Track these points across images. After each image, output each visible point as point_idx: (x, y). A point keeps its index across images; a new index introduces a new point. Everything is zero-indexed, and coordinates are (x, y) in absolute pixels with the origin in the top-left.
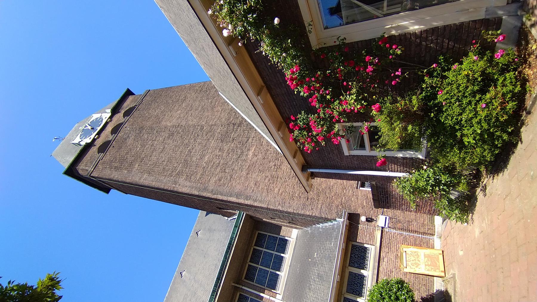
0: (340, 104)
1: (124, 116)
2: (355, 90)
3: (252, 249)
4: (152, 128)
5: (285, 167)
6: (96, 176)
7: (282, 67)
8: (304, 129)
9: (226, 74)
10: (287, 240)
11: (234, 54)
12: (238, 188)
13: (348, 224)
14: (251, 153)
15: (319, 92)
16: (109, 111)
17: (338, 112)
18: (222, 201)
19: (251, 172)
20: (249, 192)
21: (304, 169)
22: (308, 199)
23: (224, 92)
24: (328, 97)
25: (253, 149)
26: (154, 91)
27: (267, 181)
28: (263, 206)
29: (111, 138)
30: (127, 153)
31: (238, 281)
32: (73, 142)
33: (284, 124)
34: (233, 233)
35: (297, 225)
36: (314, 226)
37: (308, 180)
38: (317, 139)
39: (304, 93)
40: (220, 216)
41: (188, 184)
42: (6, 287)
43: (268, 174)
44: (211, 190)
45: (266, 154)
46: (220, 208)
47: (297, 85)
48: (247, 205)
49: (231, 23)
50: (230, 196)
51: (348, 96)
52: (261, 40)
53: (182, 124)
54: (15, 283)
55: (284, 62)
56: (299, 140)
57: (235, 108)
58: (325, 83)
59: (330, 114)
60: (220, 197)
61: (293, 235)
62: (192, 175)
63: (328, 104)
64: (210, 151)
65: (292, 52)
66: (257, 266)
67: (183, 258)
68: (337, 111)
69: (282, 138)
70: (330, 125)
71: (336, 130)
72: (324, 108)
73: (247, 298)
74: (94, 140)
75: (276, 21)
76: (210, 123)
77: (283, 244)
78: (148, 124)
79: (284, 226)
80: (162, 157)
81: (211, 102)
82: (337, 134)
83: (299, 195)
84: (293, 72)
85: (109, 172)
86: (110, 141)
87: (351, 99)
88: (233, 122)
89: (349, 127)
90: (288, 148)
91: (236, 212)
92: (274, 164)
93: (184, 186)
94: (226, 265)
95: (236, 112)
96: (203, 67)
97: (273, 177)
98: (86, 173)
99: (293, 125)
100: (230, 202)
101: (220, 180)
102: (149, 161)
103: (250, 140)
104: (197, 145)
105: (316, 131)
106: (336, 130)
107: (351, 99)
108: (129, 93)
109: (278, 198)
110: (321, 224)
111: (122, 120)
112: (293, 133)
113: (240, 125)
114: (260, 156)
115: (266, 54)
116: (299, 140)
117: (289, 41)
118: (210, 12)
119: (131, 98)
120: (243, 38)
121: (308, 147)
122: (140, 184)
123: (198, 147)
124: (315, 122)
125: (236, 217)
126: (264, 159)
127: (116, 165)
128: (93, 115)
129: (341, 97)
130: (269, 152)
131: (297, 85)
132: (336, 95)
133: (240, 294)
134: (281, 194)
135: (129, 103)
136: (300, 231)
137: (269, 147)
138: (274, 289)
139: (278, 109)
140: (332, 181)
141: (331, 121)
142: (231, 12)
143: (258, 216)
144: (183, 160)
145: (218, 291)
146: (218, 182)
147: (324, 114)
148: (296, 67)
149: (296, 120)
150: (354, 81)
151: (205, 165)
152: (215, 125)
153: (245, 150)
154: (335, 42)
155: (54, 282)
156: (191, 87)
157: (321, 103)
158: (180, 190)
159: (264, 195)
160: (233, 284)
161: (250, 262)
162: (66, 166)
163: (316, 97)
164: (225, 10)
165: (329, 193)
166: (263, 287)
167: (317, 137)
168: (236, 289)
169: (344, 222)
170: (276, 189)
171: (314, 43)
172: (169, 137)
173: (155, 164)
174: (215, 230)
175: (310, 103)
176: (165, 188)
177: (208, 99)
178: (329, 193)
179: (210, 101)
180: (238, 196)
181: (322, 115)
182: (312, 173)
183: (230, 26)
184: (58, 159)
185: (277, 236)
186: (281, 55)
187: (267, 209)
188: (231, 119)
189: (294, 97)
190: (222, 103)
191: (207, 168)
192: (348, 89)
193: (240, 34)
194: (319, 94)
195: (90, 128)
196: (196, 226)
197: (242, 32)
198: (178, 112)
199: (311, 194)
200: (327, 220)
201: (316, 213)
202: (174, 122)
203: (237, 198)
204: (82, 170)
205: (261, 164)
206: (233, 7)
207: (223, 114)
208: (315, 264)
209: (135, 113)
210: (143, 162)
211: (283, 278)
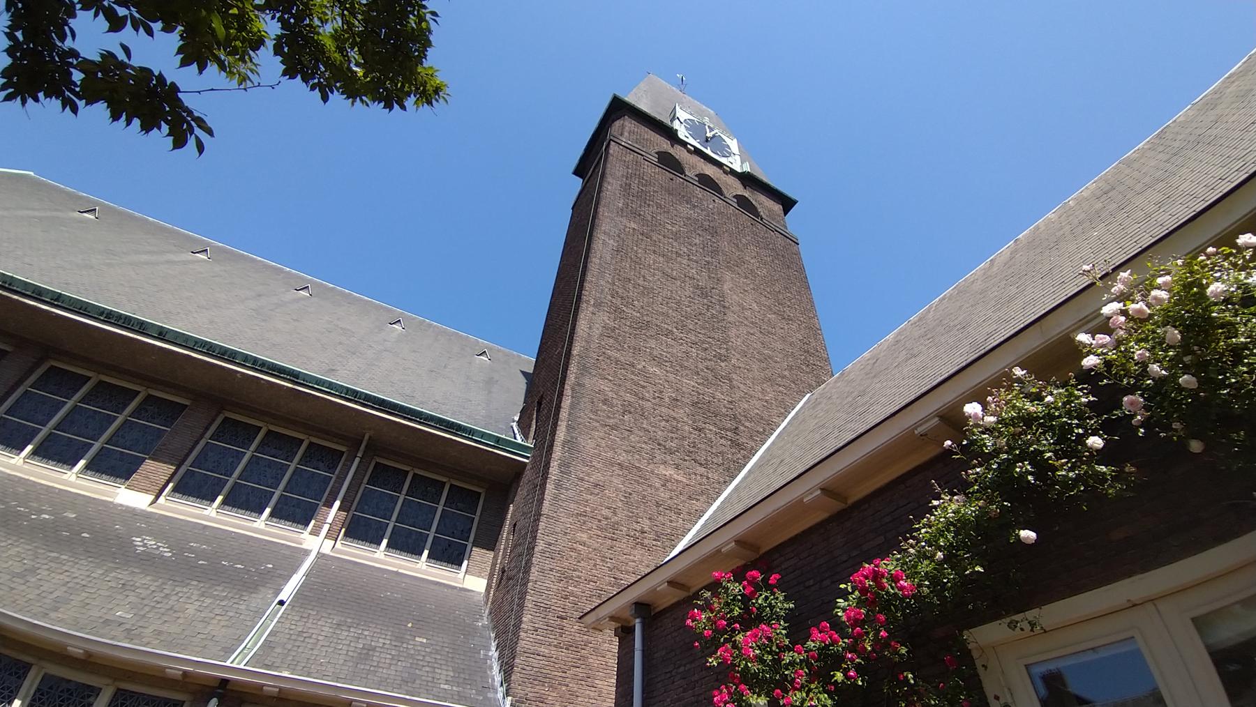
1: (736, 197)
3: (406, 468)
4: (715, 252)
5: (641, 561)
8: (746, 609)
10: (460, 565)
11: (919, 429)
12: (587, 444)
14: (670, 472)
15: (851, 648)
18: (558, 407)
20: (578, 470)
21: (642, 607)
22: (562, 618)
24: (839, 676)
25: (680, 478)
26: (798, 254)
27: (606, 512)
28: (546, 504)
29: (690, 173)
30: (659, 206)
31: (375, 448)
33: (754, 556)
34: (483, 435)
36: (493, 635)
37: (612, 618)
39: (844, 610)
40: (521, 405)
41: (596, 332)
42: (424, 7)
43: (621, 515)
44: (585, 383)
46: (540, 404)
47: (864, 591)
49: (998, 422)
50: (568, 426)
52: (966, 495)
53: (729, 314)
54: (433, 25)
55: (922, 555)
57: (776, 434)
60: (566, 402)
61: (473, 580)
62: (616, 339)
64: (671, 377)
65: (950, 575)
66: (404, 492)
67: (430, 325)
69: (719, 551)
70: (765, 680)
72: (809, 666)
73: (331, 468)
75: (1028, 535)
76: (734, 376)
77: (450, 555)
78: (725, 245)
79: (495, 558)
81: (784, 377)
83: (572, 594)
84: (895, 579)
86: (683, 172)
91: (530, 440)
93: (590, 324)
94: (410, 420)
97: (615, 526)
99: (755, 578)
100: (555, 425)
101: (605, 402)
103: (701, 470)
104: (684, 348)
105: (746, 642)
108: (787, 204)
109: (563, 542)
110: (496, 655)
111: (729, 194)
112: (736, 581)
113: (736, 444)
114: (664, 495)
115: (935, 507)
117: (978, 569)
118: (1018, 372)
119: (778, 208)
120: (964, 449)
121: (701, 620)
123: (678, 350)
124: (769, 639)
125: (519, 441)
126: (658, 505)
127: (634, 186)
130: (674, 517)
131: (864, 591)
133: (343, 453)
134: (573, 549)
136: (481, 598)
137: (686, 517)
138: (346, 535)
142: (1028, 420)
143: (522, 492)
145: (356, 402)
148: (911, 588)
149: (770, 588)
151: (639, 367)
152: (732, 387)
153: (676, 458)
154: (997, 698)
157: (819, 655)
158: (582, 315)
159: (572, 506)
160: (367, 437)
161: (415, 475)
162: (630, 98)
163: (835, 642)
164: (1030, 407)
166: (353, 508)
167: (729, 646)
168: (355, 444)
170: (584, 537)
171: (986, 636)
172: (697, 287)
173: (637, 262)
174: (490, 392)
176: (587, 285)
179: (786, 373)
180: (570, 444)
182: (632, 630)
183: (993, 419)
184: (642, 85)
185: (471, 539)
186: (940, 548)
188: (747, 424)
189: (827, 582)
190: (783, 401)
191: (633, 373)
193: (973, 443)
195: (709, 135)
196: (499, 351)
197: (981, 447)
199: (573, 627)
200: (507, 670)
201: (526, 641)
202: (733, 298)
203: (565, 443)
204: (623, 126)
205: (644, 497)
206: (1041, 425)
207: (758, 404)
208: (400, 639)
209: (745, 218)
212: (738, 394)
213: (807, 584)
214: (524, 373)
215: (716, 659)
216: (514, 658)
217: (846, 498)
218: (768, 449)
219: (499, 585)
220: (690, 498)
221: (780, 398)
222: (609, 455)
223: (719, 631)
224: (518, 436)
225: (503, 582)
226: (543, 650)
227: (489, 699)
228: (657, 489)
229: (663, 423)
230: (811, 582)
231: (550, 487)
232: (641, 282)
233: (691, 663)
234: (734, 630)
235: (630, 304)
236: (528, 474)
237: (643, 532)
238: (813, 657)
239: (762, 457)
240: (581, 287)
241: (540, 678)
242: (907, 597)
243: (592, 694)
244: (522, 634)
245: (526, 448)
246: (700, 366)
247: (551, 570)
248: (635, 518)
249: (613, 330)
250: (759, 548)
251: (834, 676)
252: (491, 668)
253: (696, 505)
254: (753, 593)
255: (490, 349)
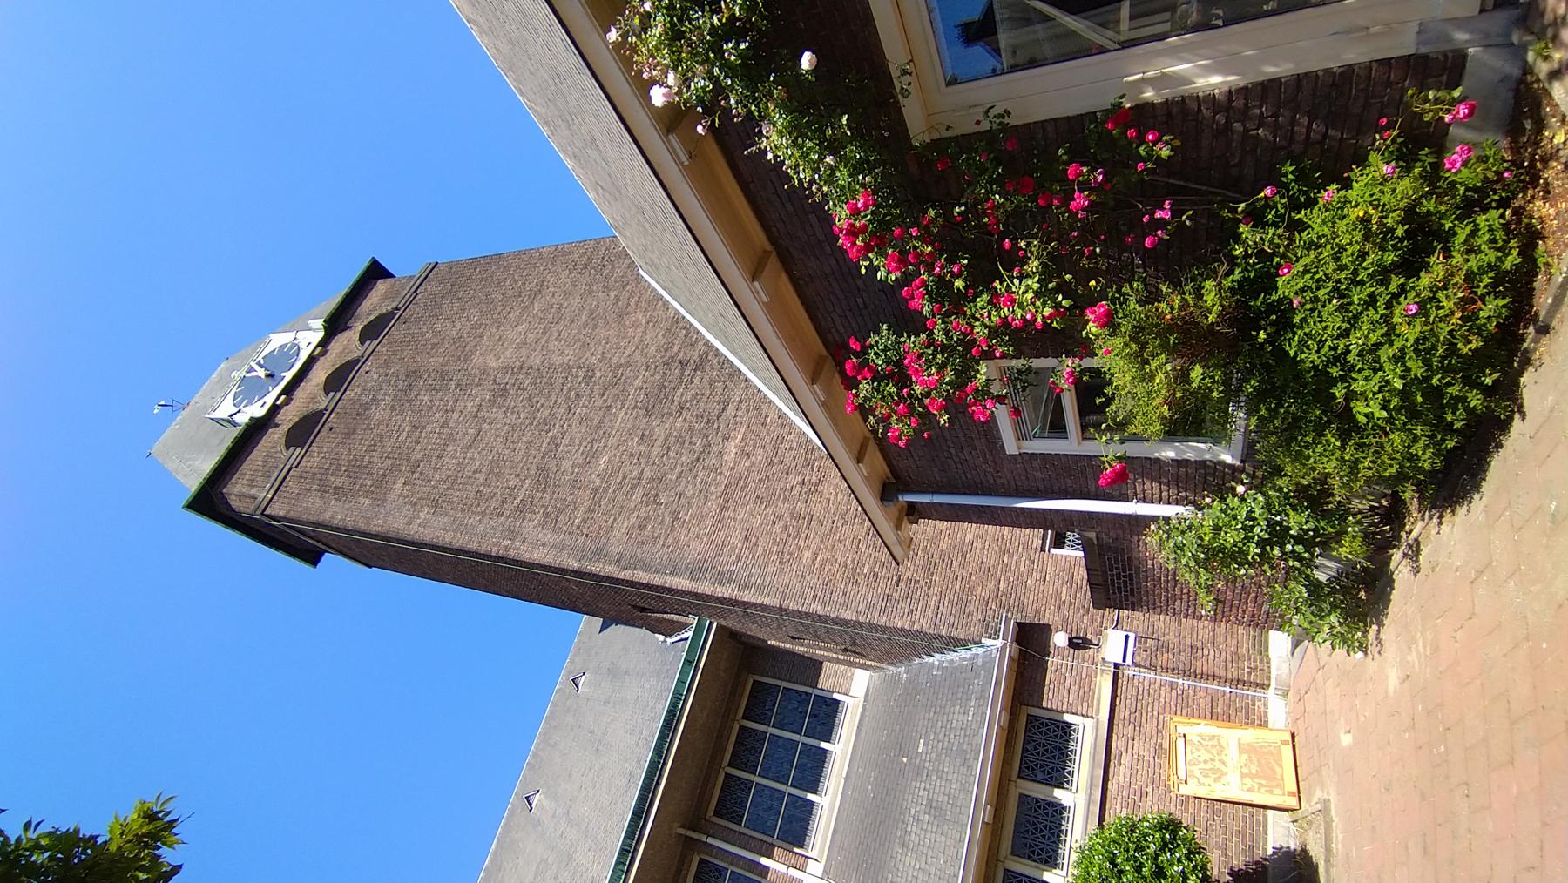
0: (993, 303)
1: (362, 340)
2: (1036, 263)
3: (737, 727)
4: (443, 376)
5: (834, 487)
6: (282, 513)
7: (824, 195)
8: (889, 377)
9: (660, 216)
10: (838, 702)
11: (684, 159)
12: (695, 549)
13: (1016, 655)
14: (732, 448)
15: (930, 269)
16: (318, 324)
17: (986, 326)
18: (648, 586)
19: (732, 502)
20: (727, 561)
21: (887, 493)
22: (899, 580)
23: (654, 269)
24: (959, 283)
25: (740, 436)
26: (450, 265)
27: (778, 528)
28: (767, 601)
29: (323, 402)
30: (371, 448)
31: (696, 821)
32: (213, 415)
33: (830, 363)
34: (681, 681)
35: (867, 657)
36: (917, 661)
37: (898, 527)
38: (925, 407)
39: (889, 272)
40: (643, 632)
41: (549, 537)
43: (783, 509)
44: (616, 554)
45: (776, 449)
46: (643, 610)
47: (868, 248)
48: (721, 600)
49: (675, 69)
50: (672, 574)
51: (1016, 281)
52: (762, 118)
53: (530, 362)
54: (45, 828)
55: (830, 181)
56: (872, 411)
57: (688, 316)
58: (950, 242)
59: (965, 334)
60: (642, 576)
61: (854, 686)
62: (560, 511)
63: (957, 304)
64: (612, 441)
65: (853, 152)
66: (751, 777)
67: (535, 755)
68: (983, 324)
69: (824, 404)
70: (962, 364)
71: (981, 379)
72: (947, 314)
73: (721, 872)
74: (275, 409)
75: (807, 61)
76: (614, 360)
77: (826, 714)
78: (433, 362)
79: (831, 660)
80: (473, 459)
81: (617, 298)
82: (985, 392)
83: (872, 569)
84: (855, 212)
85: (319, 503)
86: (321, 413)
87: (1025, 289)
88: (681, 356)
89: (1020, 372)
90: (840, 432)
91: (689, 620)
92: (799, 479)
93: (538, 545)
94: (660, 776)
95: (689, 328)
96: (591, 195)
97: (796, 517)
98: (252, 507)
99: (854, 367)
100: (671, 590)
101: (642, 527)
102: (436, 469)
103: (731, 409)
104: (574, 423)
105: (922, 383)
106: (981, 379)
107: (1025, 289)
108: (376, 272)
109: (813, 580)
110: (938, 656)
111: (356, 350)
112: (857, 388)
113: (700, 365)
114: (760, 456)
115: (776, 157)
116: (872, 411)
117: (844, 120)
118: (613, 36)
119: (381, 286)
120: (708, 112)
121: (901, 428)
122: (409, 538)
123: (578, 431)
124: (920, 356)
125: (690, 634)
126: (771, 463)
127: (339, 482)
128: (272, 336)
129: (997, 284)
130: (786, 444)
131: (868, 248)
132: (982, 279)
133: (702, 861)
134: (822, 568)
135: (376, 301)
136: (876, 675)
137: (787, 429)
138: (801, 846)
139: (813, 318)
140: (970, 530)
141: (966, 354)
142: (675, 35)
143: (754, 630)
144: (534, 467)
145: (636, 850)
146: (636, 531)
147: (946, 332)
148: (865, 195)
149: (865, 350)
150: (1035, 237)
151: (598, 481)
152: (628, 365)
153: (715, 439)
154: (978, 123)
155: (158, 826)
156: (559, 254)
157: (937, 302)
158: (526, 556)
159: (770, 569)
160: (682, 831)
161: (730, 765)
162: (193, 485)
163: (924, 284)
164: (657, 30)
165: (962, 566)
166: (769, 840)
167: (927, 401)
168: (689, 845)
169: (1003, 648)
170: (807, 554)
171: (918, 125)
172: (492, 402)
173: (453, 481)
174: (626, 672)
175: (906, 301)
176: (483, 550)
177: (607, 289)
178: (962, 566)
179: (612, 295)
180: (694, 573)
181: (940, 337)
182: (911, 505)
183: (671, 76)
184: (171, 465)
185: (808, 690)
186: (821, 160)
187: (780, 610)
188: (676, 349)
189: (860, 282)
190: (648, 302)
191: (606, 490)
192: (1015, 261)
193: (700, 101)
194: (930, 274)
195: (261, 373)
196: (572, 661)
197: (705, 93)
198: (520, 328)
199: (909, 568)
200: (953, 643)
201: (923, 624)
202: (509, 355)
203: (692, 578)
204: (241, 496)
205: (761, 480)
206: (681, 21)
207: (651, 334)
208: (919, 771)
209: (396, 332)
210: (417, 475)
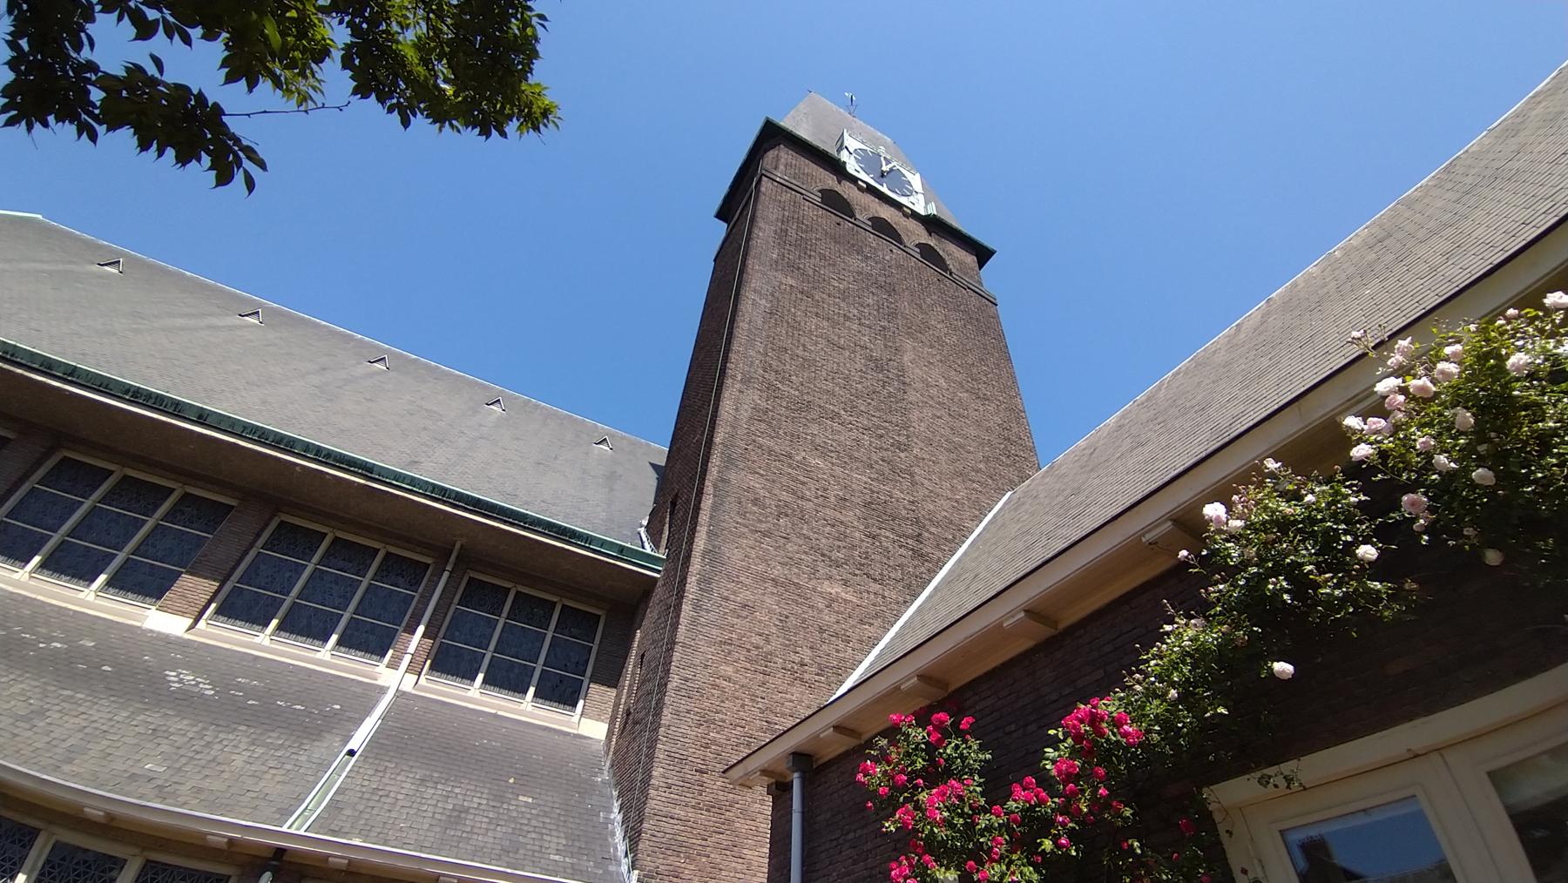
1: (919, 245)
3: (507, 585)
4: (892, 315)
5: (801, 701)
8: (932, 761)
10: (574, 705)
11: (1148, 536)
12: (733, 555)
14: (836, 589)
15: (1063, 810)
18: (697, 509)
20: (722, 586)
21: (801, 759)
22: (701, 772)
24: (1048, 844)
25: (848, 597)
26: (996, 317)
27: (756, 640)
28: (682, 629)
29: (862, 217)
30: (823, 257)
31: (468, 559)
33: (941, 695)
34: (603, 543)
36: (615, 793)
37: (765, 772)
39: (1054, 762)
40: (650, 506)
41: (745, 414)
43: (776, 643)
44: (730, 479)
46: (674, 504)
47: (1078, 738)
49: (1246, 527)
50: (709, 533)
52: (1206, 618)
53: (911, 392)
55: (1151, 694)
57: (968, 542)
60: (707, 503)
61: (590, 724)
62: (769, 424)
64: (838, 470)
65: (1186, 719)
66: (505, 614)
67: (537, 406)
69: (897, 688)
70: (954, 850)
72: (1010, 831)
73: (414, 585)
75: (1283, 668)
76: (917, 470)
77: (562, 693)
78: (905, 306)
79: (618, 697)
81: (978, 471)
83: (714, 742)
84: (1117, 723)
86: (852, 215)
91: (662, 550)
93: (737, 405)
94: (512, 524)
97: (768, 657)
99: (942, 722)
100: (693, 531)
101: (755, 502)
103: (876, 587)
104: (854, 434)
105: (932, 802)
108: (983, 254)
109: (703, 677)
110: (619, 818)
111: (910, 242)
112: (918, 725)
113: (918, 555)
114: (828, 618)
115: (1168, 634)
117: (1221, 710)
118: (1271, 465)
119: (971, 260)
120: (1203, 561)
121: (875, 774)
123: (846, 437)
124: (960, 798)
125: (648, 551)
126: (821, 631)
127: (792, 232)
130: (842, 646)
131: (1078, 738)
133: (428, 566)
134: (715, 686)
136: (601, 747)
137: (857, 646)
138: (432, 668)
142: (1284, 525)
143: (651, 615)
145: (444, 503)
148: (1138, 734)
149: (961, 734)
151: (798, 458)
152: (914, 483)
153: (844, 572)
154: (1244, 872)
155: (535, 117)
157: (1023, 818)
158: (726, 394)
159: (714, 632)
160: (458, 546)
161: (518, 593)
162: (786, 123)
163: (1042, 802)
164: (1286, 508)
166: (441, 634)
167: (910, 807)
168: (443, 554)
170: (729, 670)
171: (1231, 795)
172: (870, 359)
173: (795, 327)
174: (612, 490)
176: (732, 356)
179: (981, 466)
180: (711, 554)
182: (789, 787)
183: (1239, 523)
184: (802, 106)
185: (588, 673)
186: (1173, 685)
188: (933, 530)
189: (1033, 727)
190: (977, 501)
191: (790, 466)
193: (1214, 553)
195: (885, 168)
196: (623, 438)
197: (1225, 558)
199: (715, 783)
200: (633, 837)
201: (656, 801)
202: (915, 372)
203: (705, 553)
204: (778, 158)
205: (804, 621)
206: (1299, 531)
207: (946, 504)
208: (500, 798)
209: (930, 273)
211: (566, 718)
212: (922, 492)
213: (1008, 729)
214: (654, 466)
215: (894, 823)
216: (641, 822)
217: (1056, 622)
218: (959, 560)
219: (622, 731)
220: (861, 622)
221: (973, 497)
222: (761, 568)
223: (898, 789)
224: (647, 545)
225: (628, 727)
226: (678, 811)
227: (611, 873)
228: (821, 611)
229: (828, 529)
230: (1013, 727)
231: (686, 608)
232: (800, 352)
233: (863, 827)
234: (916, 787)
235: (787, 380)
236: (659, 592)
237: (803, 665)
238: (1015, 821)
239: (951, 571)
240: (726, 359)
241: (674, 847)
242: (1133, 745)
243: (739, 867)
244: (652, 792)
245: (656, 560)
246: (874, 457)
247: (688, 712)
248: (793, 647)
249: (766, 412)
250: (947, 685)
251: (1041, 844)
252: (613, 834)
253: (870, 631)
254: (940, 741)
255: (612, 436)
